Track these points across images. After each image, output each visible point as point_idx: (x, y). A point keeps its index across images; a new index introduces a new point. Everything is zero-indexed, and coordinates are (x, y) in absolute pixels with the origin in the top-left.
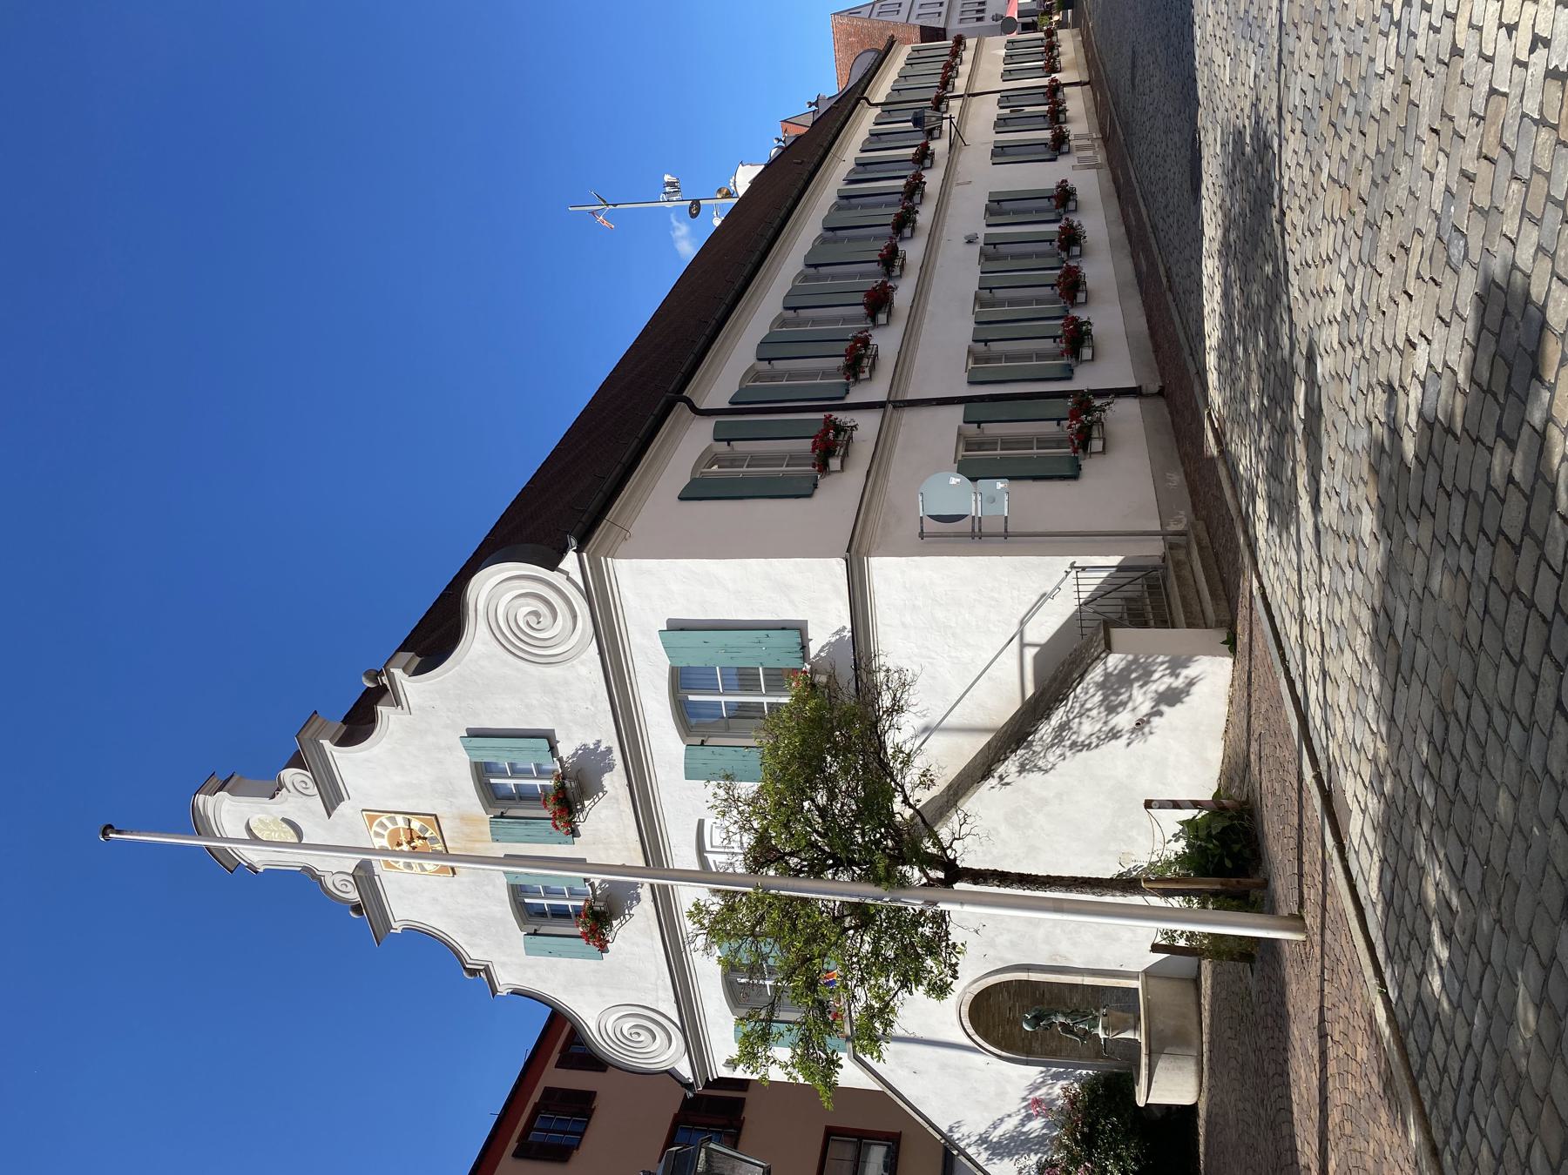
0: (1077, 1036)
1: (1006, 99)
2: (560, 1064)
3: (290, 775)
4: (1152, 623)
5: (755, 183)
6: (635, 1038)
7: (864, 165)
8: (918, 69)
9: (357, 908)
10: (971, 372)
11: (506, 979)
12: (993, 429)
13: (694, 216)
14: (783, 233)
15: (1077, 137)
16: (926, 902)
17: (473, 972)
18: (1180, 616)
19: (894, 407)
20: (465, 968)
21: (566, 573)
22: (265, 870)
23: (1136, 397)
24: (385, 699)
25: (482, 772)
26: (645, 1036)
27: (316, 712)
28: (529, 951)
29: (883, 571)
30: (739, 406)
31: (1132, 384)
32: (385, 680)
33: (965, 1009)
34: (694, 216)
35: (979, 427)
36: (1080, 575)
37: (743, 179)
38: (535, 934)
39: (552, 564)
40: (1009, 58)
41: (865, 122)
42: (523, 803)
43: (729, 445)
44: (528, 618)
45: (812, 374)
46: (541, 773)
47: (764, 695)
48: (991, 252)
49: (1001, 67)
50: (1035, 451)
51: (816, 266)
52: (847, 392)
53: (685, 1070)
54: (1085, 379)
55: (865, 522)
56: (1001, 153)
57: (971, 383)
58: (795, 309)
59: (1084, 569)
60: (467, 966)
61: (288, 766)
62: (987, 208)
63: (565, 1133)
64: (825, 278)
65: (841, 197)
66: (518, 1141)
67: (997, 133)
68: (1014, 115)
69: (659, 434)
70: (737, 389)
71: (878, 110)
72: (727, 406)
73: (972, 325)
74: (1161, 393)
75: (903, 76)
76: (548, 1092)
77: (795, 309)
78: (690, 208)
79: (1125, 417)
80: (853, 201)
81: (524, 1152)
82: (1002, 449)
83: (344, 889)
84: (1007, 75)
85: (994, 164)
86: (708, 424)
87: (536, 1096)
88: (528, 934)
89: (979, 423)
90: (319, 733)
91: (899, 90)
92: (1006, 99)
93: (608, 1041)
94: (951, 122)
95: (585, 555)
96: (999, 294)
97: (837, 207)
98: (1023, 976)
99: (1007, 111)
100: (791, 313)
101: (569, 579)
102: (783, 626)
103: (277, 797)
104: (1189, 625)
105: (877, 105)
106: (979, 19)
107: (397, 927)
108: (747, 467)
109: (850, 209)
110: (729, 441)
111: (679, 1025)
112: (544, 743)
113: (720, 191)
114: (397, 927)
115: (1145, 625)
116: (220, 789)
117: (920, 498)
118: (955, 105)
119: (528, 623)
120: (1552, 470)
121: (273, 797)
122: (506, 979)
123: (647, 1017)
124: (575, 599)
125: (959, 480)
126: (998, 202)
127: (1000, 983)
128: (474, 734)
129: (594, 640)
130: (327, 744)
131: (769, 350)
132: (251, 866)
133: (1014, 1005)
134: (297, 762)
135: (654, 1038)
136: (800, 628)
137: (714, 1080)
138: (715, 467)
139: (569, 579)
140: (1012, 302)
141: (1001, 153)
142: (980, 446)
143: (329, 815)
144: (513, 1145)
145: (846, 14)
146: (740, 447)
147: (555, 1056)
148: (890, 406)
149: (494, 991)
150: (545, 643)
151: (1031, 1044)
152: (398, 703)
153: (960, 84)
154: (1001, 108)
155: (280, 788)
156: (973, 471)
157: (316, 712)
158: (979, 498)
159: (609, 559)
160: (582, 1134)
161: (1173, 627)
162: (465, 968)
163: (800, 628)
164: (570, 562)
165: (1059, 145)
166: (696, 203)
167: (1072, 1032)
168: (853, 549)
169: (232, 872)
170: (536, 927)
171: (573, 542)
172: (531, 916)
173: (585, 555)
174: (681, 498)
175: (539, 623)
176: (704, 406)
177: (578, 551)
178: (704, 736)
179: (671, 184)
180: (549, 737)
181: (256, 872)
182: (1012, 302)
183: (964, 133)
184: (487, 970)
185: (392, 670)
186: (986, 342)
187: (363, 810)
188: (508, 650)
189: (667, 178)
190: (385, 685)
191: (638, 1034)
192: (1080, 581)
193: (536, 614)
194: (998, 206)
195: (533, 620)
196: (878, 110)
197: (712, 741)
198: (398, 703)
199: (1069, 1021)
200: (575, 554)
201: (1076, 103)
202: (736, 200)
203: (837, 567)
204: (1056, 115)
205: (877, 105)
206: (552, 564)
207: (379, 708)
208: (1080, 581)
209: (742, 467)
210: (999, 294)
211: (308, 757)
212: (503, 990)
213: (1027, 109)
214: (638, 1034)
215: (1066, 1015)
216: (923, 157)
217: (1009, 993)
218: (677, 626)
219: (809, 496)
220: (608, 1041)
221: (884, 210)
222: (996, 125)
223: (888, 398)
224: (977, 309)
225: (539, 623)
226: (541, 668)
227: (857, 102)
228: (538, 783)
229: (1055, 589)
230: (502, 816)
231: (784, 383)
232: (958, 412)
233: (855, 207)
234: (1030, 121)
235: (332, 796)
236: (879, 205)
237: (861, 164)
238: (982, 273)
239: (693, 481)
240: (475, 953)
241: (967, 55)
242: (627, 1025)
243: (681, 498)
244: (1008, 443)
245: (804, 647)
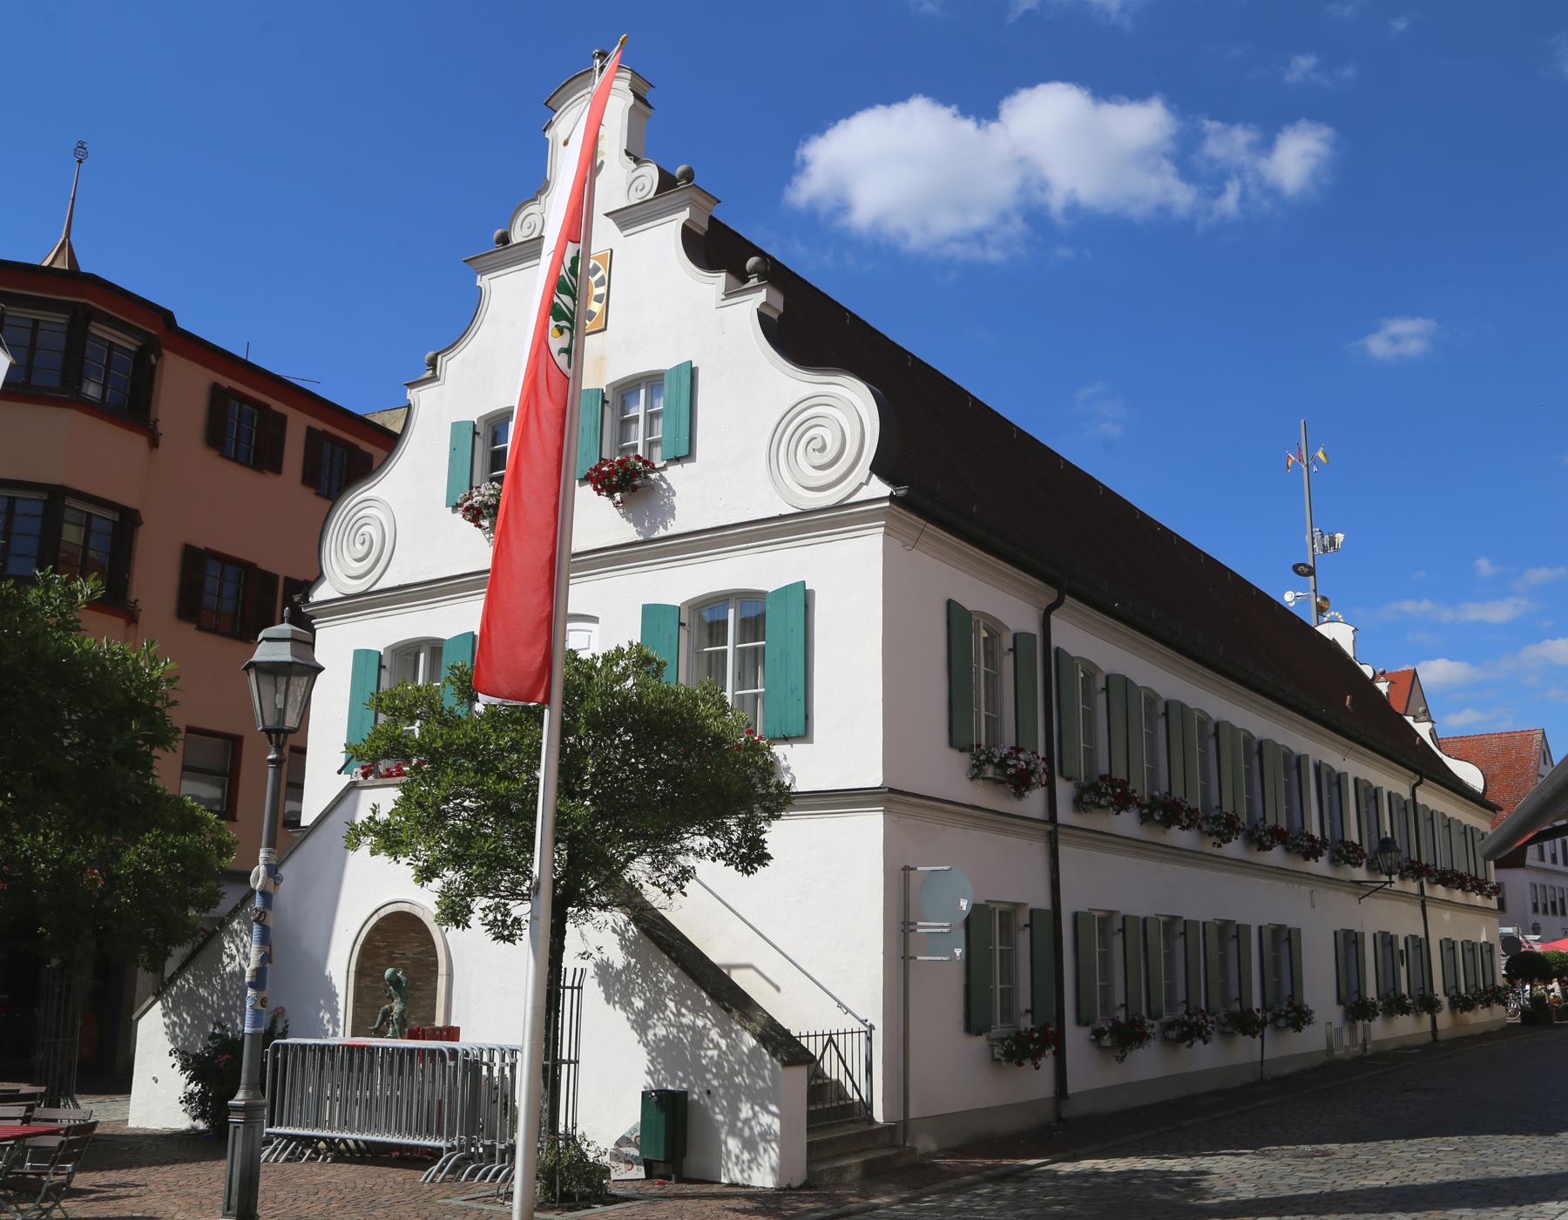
0: (381, 1024)
1: (1420, 945)
2: (310, 431)
3: (651, 174)
4: (812, 1108)
5: (1333, 647)
6: (359, 539)
7: (1339, 783)
8: (1458, 841)
9: (504, 239)
10: (1089, 915)
11: (422, 398)
12: (1023, 940)
13: (1295, 568)
14: (1258, 696)
15: (1366, 1029)
16: (538, 883)
17: (433, 364)
18: (818, 1138)
19: (1050, 833)
20: (437, 354)
21: (867, 483)
22: (547, 139)
23: (1056, 1092)
24: (733, 280)
25: (652, 381)
26: (361, 550)
27: (719, 202)
28: (457, 427)
29: (870, 825)
30: (1055, 660)
31: (1071, 1090)
32: (754, 282)
33: (405, 908)
34: (1295, 568)
35: (1026, 926)
36: (863, 1035)
37: (1338, 632)
38: (475, 433)
39: (878, 468)
40: (1470, 946)
41: (1391, 781)
42: (618, 425)
43: (1010, 650)
44: (819, 439)
45: (1090, 737)
46: (650, 445)
47: (733, 692)
48: (1229, 932)
49: (1458, 938)
50: (999, 987)
51: (1217, 734)
52: (1069, 779)
53: (321, 594)
54: (1076, 1038)
55: (924, 806)
56: (1349, 942)
57: (1076, 916)
58: (1166, 714)
59: (869, 1039)
60: (439, 357)
61: (662, 172)
62: (1281, 927)
63: (237, 440)
64: (1203, 745)
65: (1299, 758)
66: (230, 388)
67: (1375, 935)
68: (1395, 953)
69: (1022, 573)
70: (1073, 655)
71: (1406, 795)
72: (1055, 643)
73: (1141, 914)
74: (1060, 1119)
75: (1449, 823)
76: (282, 419)
77: (1166, 714)
78: (1304, 565)
79: (1035, 1082)
80: (1294, 774)
81: (217, 394)
82: (1001, 951)
83: (526, 224)
84: (1448, 946)
85: (1335, 932)
86: (1031, 625)
87: (276, 406)
88: (474, 425)
89: (1030, 926)
90: (693, 204)
91: (1432, 819)
92: (1420, 945)
93: (354, 520)
94: (1386, 883)
95: (887, 504)
96: (1180, 943)
97: (1288, 754)
98: (442, 969)
99: (1402, 946)
100: (1161, 709)
101: (862, 485)
102: (808, 717)
103: (627, 158)
104: (810, 1145)
105: (1413, 794)
106: (1535, 906)
107: (483, 281)
108: (986, 672)
109: (1285, 768)
110: (1014, 650)
111: (372, 589)
112: (684, 452)
113: (1324, 599)
114: (483, 281)
115: (810, 1101)
116: (637, 96)
117: (945, 868)
118: (1413, 887)
119: (815, 438)
120: (622, 53)
121: (628, 153)
122: (422, 398)
123: (380, 555)
124: (839, 491)
125: (964, 908)
126: (1289, 939)
127: (433, 943)
128: (693, 373)
129: (795, 511)
130: (684, 215)
131: (1119, 687)
132: (550, 124)
133: (408, 958)
134: (667, 183)
135: (359, 560)
136: (805, 735)
137: (313, 625)
138: (985, 635)
139: (862, 485)
140: (1170, 957)
141: (1349, 942)
142: (1103, 932)
143: (607, 215)
144: (226, 382)
145: (1544, 747)
146: (1007, 663)
147: (319, 425)
148: (1422, 898)
149: (411, 385)
150: (792, 456)
151: (370, 975)
152: (729, 294)
153: (1440, 891)
154: (1406, 939)
155: (636, 160)
156: (976, 923)
157: (719, 202)
158: (945, 930)
159: (882, 529)
160: (235, 460)
161: (808, 1129)
162: (437, 354)
163: (805, 735)
164: (879, 488)
165: (1357, 1010)
166: (1311, 572)
167: (383, 1019)
168: (892, 795)
169: (546, 104)
170: (482, 434)
171: (902, 492)
172: (494, 428)
173: (887, 504)
174: (950, 604)
175: (814, 450)
176: (1054, 619)
177: (891, 498)
178: (689, 626)
179: (1332, 542)
180: (689, 456)
181: (545, 130)
182: (1170, 957)
183: (1374, 897)
184: (434, 378)
185: (764, 291)
186: (1123, 930)
187: (612, 251)
188: (783, 418)
189: (1340, 537)
190: (748, 280)
191: (363, 543)
192: (856, 1035)
193: (823, 449)
194: (1283, 940)
195: (817, 444)
196: (1406, 795)
197: (684, 634)
198: (729, 294)
199: (395, 1016)
200: (888, 494)
201: (1407, 1027)
202: (1313, 623)
203: (873, 777)
204: (1395, 1005)
205: (1413, 794)
206: (878, 468)
207: (723, 275)
208: (856, 1035)
209: (986, 666)
210: (1180, 943)
211: (671, 197)
212: (412, 395)
213: (1403, 970)
214: (363, 543)
215: (402, 1013)
216: (1346, 854)
217: (420, 953)
218: (807, 599)
219: (952, 744)
220: (354, 520)
221: (1283, 808)
222: (1385, 934)
223: (1060, 825)
224: (1161, 919)
225: (814, 450)
226: (766, 449)
227: (1416, 772)
228: (640, 443)
229: (845, 1008)
230: (604, 402)
231: (1081, 706)
232: (1042, 901)
233: (1287, 775)
234: (1387, 975)
235: (626, 218)
236: (1289, 802)
237: (1339, 780)
238: (1204, 923)
239: (969, 613)
240: (451, 365)
241: (1477, 900)
242: (372, 530)
243: (950, 604)
244: (1008, 957)
245: (786, 739)
